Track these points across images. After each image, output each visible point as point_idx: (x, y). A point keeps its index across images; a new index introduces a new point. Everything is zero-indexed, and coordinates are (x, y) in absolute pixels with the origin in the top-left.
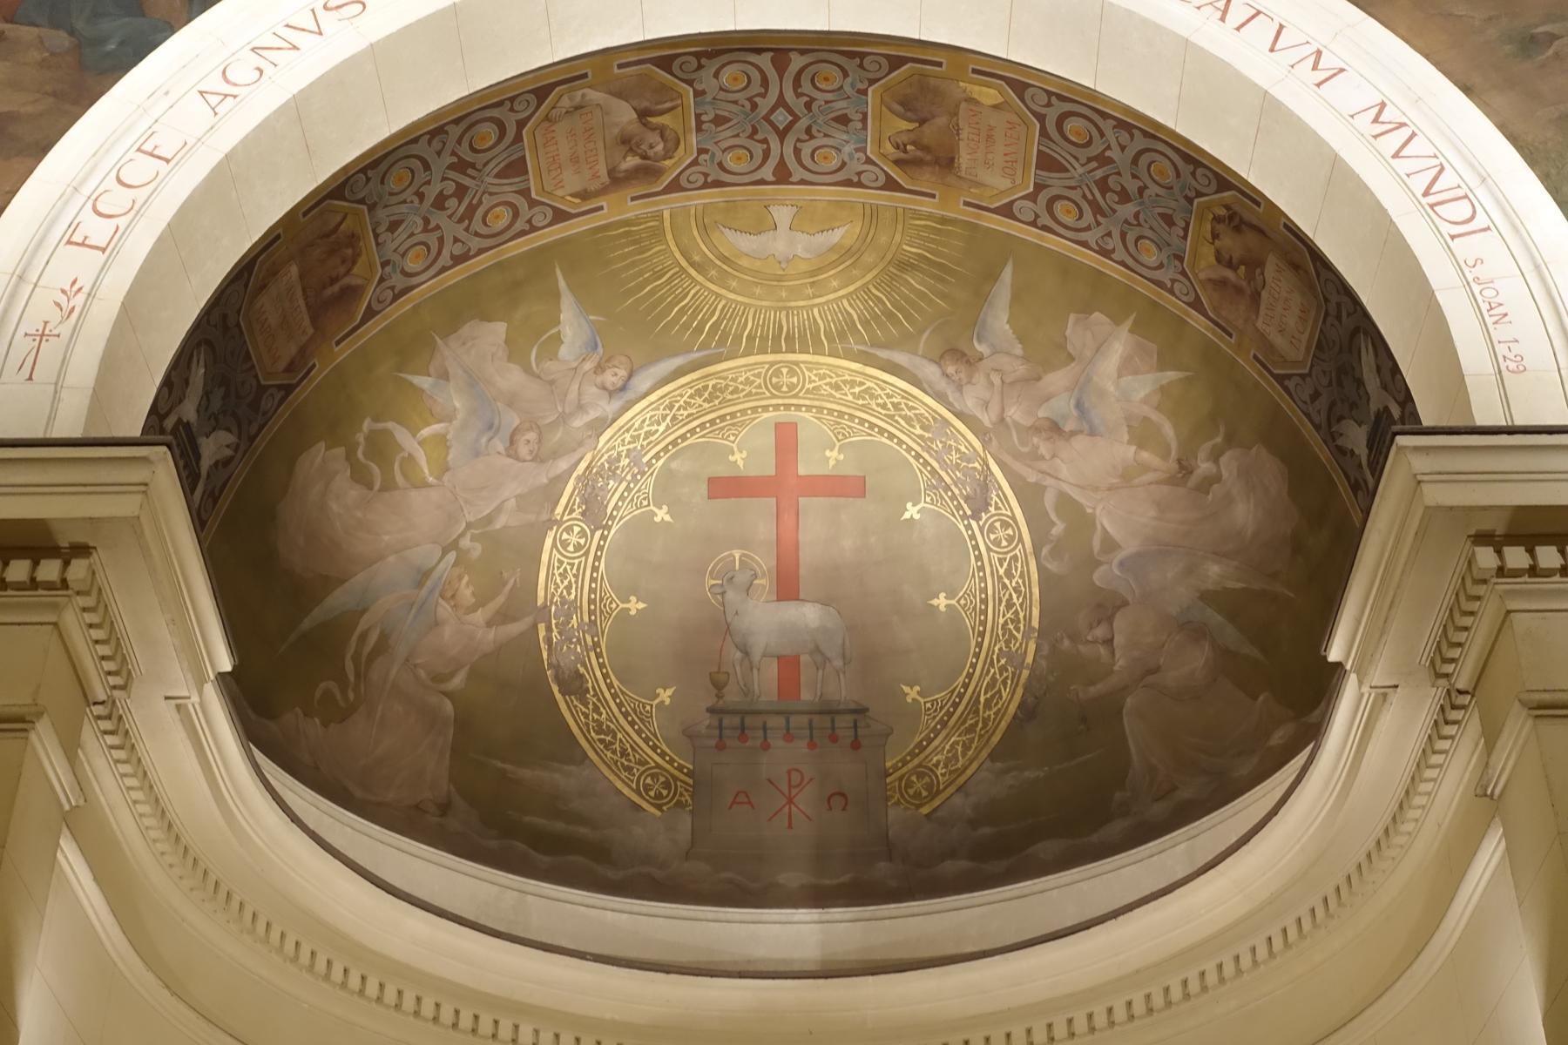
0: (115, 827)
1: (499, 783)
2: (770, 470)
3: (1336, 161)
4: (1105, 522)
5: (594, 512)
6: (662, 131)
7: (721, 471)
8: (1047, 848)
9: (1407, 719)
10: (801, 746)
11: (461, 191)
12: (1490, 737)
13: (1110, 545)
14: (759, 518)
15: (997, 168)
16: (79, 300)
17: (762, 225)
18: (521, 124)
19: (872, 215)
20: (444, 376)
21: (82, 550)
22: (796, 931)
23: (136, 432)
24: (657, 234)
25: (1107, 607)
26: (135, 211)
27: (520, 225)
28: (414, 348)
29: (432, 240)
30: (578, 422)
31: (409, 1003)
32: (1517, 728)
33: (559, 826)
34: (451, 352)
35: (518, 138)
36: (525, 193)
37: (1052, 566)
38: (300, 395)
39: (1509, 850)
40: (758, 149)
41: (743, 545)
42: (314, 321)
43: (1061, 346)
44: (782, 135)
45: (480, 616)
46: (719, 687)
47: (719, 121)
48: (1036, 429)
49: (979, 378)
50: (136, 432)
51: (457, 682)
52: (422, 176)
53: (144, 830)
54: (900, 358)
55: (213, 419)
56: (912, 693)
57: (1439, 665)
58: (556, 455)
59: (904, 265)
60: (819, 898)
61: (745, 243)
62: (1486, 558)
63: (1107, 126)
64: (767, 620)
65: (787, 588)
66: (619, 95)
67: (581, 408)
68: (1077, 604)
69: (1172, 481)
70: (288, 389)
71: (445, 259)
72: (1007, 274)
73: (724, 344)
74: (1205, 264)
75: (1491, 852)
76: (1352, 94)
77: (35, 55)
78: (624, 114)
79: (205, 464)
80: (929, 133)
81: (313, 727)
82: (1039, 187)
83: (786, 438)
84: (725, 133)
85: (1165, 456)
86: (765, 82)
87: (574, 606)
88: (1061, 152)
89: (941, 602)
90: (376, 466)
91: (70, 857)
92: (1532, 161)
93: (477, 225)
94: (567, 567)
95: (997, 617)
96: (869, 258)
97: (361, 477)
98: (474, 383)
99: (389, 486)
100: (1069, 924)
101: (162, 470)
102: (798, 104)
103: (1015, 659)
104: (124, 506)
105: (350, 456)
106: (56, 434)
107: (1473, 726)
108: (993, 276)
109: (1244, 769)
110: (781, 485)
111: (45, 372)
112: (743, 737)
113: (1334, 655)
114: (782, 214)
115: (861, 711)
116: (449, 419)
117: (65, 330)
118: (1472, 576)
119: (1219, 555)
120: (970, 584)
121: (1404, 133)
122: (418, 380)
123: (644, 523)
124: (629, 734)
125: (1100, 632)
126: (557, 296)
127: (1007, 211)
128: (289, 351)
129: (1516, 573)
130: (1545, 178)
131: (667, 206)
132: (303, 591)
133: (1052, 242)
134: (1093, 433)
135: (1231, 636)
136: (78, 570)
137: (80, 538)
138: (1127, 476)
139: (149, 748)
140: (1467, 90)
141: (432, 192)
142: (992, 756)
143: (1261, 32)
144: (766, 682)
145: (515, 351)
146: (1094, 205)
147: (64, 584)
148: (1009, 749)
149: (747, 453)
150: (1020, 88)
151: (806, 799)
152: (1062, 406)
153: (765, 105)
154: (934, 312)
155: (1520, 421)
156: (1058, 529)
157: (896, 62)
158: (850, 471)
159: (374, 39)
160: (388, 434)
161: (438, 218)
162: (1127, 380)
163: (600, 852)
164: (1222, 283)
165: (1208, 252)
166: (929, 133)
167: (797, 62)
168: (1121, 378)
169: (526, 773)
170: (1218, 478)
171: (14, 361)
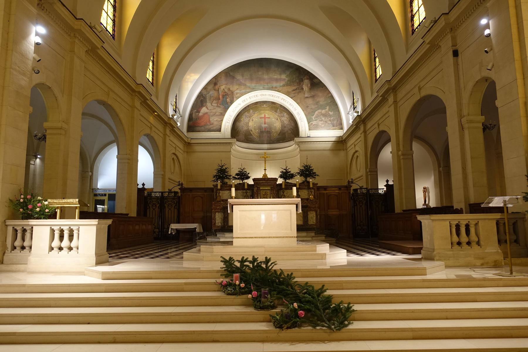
0: (260, 242)
1: (248, 138)
5: (253, 120)
14: (263, 120)
22: (265, 146)
25: (285, 127)
60: (267, 144)
64: (264, 126)
65: (265, 124)
68: (283, 126)
73: (261, 110)
83: (265, 115)
124: (255, 134)
144: (264, 130)
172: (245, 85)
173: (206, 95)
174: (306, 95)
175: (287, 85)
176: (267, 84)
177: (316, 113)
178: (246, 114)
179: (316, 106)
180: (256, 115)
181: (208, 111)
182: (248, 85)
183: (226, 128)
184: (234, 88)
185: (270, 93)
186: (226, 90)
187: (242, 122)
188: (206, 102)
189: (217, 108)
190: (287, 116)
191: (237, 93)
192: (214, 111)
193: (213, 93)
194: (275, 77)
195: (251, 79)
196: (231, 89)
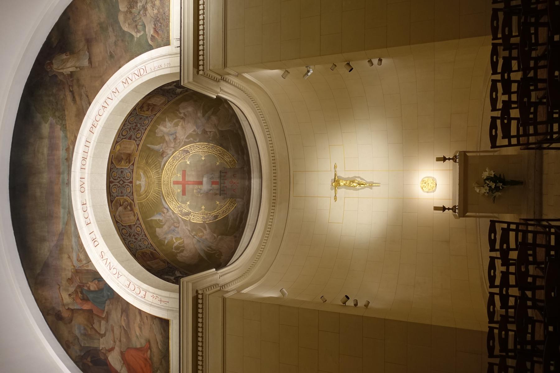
1: (230, 230)
3: (132, 91)
4: (191, 131)
5: (188, 214)
6: (123, 202)
7: (181, 193)
8: (243, 143)
9: (225, 86)
10: (226, 181)
11: (134, 235)
12: (229, 74)
13: (194, 131)
14: (189, 187)
15: (130, 147)
16: (155, 295)
17: (140, 186)
18: (122, 226)
19: (138, 167)
20: (165, 238)
21: (197, 291)
22: (255, 182)
23: (178, 286)
24: (141, 203)
25: (205, 132)
26: (139, 287)
27: (140, 226)
28: (160, 243)
29: (142, 240)
30: (173, 216)
31: (265, 241)
32: (228, 70)
33: (238, 219)
34: (161, 237)
35: (125, 226)
36: (134, 225)
37: (198, 140)
38: (169, 261)
39: (246, 73)
40: (127, 186)
41: (193, 190)
42: (157, 259)
43: (161, 137)
44: (124, 182)
45: (205, 232)
46: (216, 194)
47: (122, 193)
48: (175, 142)
49: (166, 151)
50: (178, 286)
51: (215, 235)
52: (131, 242)
53: (240, 282)
54: (163, 164)
55: (173, 274)
56: (218, 163)
57: (217, 81)
58: (178, 220)
59: (147, 163)
60: (250, 179)
61: (143, 189)
62: (201, 72)
63: (124, 128)
64: (206, 186)
65: (201, 183)
66: (117, 209)
67: (170, 216)
68: (204, 137)
69: (184, 121)
70: (168, 263)
71: (146, 238)
72: (149, 146)
73: (160, 193)
74: (149, 113)
75: (246, 75)
76: (121, 87)
77: (111, 306)
78: (120, 209)
79: (181, 275)
80: (124, 157)
81: (223, 257)
82: (134, 140)
83: (176, 183)
84: (124, 192)
86: (115, 185)
87: (203, 217)
88: (128, 136)
89: (203, 158)
90: (180, 248)
91: (245, 291)
92: (133, 58)
93: (140, 233)
94: (197, 218)
95: (206, 150)
96: (146, 168)
97: (182, 251)
98: (166, 233)
99: (183, 247)
101: (184, 280)
102: (119, 180)
103: (213, 147)
104: (190, 285)
105: (179, 253)
106: (178, 297)
107: (227, 76)
108: (149, 148)
109: (231, 111)
110: (184, 184)
111: (167, 300)
112: (224, 190)
113: (215, 97)
114: (138, 183)
115: (221, 172)
116: (172, 238)
117: (160, 297)
118: (205, 75)
120: (200, 153)
121: (128, 79)
122: (166, 242)
123: (190, 206)
124: (224, 208)
125: (209, 133)
126: (151, 220)
127: (138, 145)
128: (162, 263)
129: (203, 68)
130: (136, 56)
131: (136, 202)
132: (201, 259)
133: (144, 138)
134: (176, 133)
135: (210, 112)
136: (200, 292)
137: (195, 292)
138: (183, 128)
139: (227, 281)
140: (120, 68)
141: (135, 240)
142: (228, 151)
143: (109, 101)
145: (161, 227)
146: (137, 131)
147: (202, 294)
148: (227, 149)
149: (178, 189)
150: (117, 142)
151: (235, 181)
152: (171, 138)
153: (119, 185)
154: (155, 158)
155: (179, 65)
156: (192, 139)
157: (112, 163)
158: (181, 173)
160: (175, 247)
161: (139, 239)
162: (167, 127)
163: (242, 213)
164: (152, 110)
165: (147, 112)
166: (124, 157)
167: (112, 179)
168: (167, 128)
169: (230, 224)
170: (184, 113)
171: (165, 305)
172: (61, 234)
173: (82, 348)
174: (86, 63)
175: (62, 118)
176: (59, 173)
177: (126, 28)
179: (110, 29)
181: (117, 349)
183: (157, 301)
184: (67, 266)
186: (72, 289)
187: (187, 241)
188: (97, 350)
189: (111, 322)
190: (168, 124)
191: (79, 260)
192: (117, 331)
193: (78, 325)
194: (46, 151)
195: (49, 217)
196: (69, 275)
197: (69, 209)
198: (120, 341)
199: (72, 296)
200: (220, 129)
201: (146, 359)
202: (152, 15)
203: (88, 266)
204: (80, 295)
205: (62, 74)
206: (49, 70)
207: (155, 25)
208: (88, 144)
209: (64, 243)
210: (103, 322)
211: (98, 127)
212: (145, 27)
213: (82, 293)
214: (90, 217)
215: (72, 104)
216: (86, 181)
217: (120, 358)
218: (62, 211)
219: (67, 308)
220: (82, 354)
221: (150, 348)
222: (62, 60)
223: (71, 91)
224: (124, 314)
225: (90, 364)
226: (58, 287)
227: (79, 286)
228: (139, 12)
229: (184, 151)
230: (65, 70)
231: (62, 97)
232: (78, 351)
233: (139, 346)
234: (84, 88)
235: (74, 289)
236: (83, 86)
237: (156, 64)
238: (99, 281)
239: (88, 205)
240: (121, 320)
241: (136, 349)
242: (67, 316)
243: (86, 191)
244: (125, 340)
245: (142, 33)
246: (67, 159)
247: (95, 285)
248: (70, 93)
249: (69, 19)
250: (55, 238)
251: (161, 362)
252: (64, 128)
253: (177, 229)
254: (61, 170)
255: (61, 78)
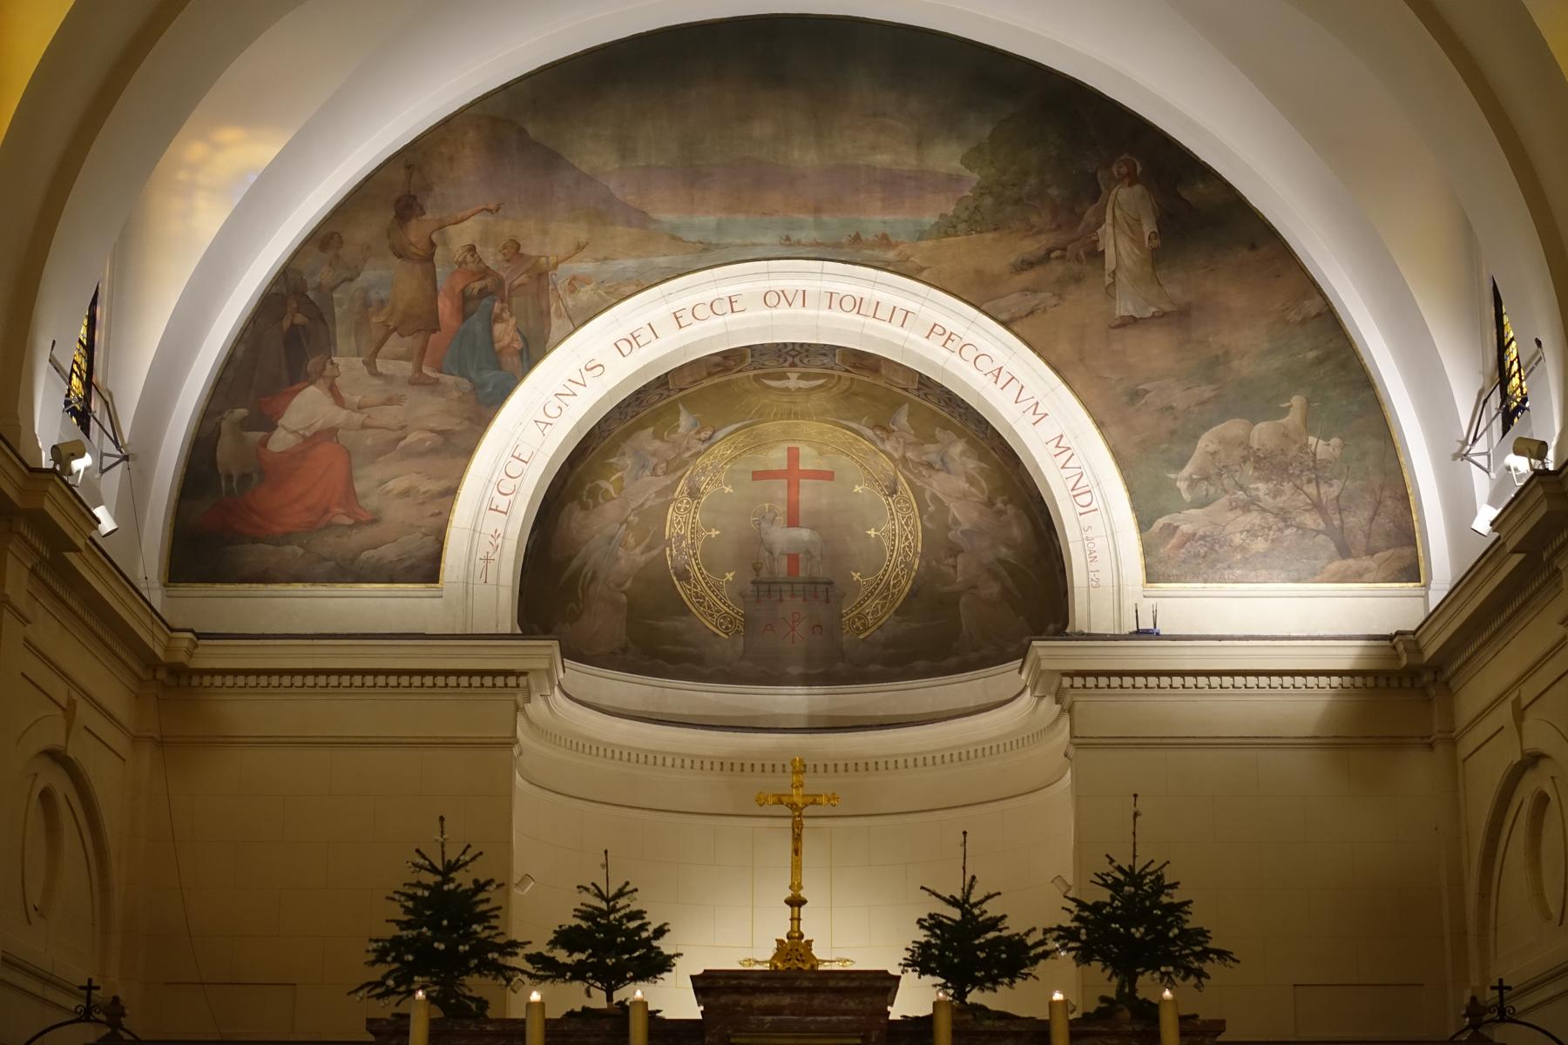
2: (784, 466)
5: (694, 493)
8: (921, 664)
10: (799, 601)
13: (956, 522)
14: (779, 489)
22: (795, 700)
25: (954, 551)
33: (678, 649)
37: (928, 525)
45: (638, 550)
46: (757, 570)
51: (628, 585)
56: (856, 576)
60: (807, 680)
64: (781, 536)
65: (793, 521)
68: (941, 545)
77: (456, 395)
83: (793, 455)
85: (983, 492)
87: (683, 537)
89: (872, 533)
94: (679, 521)
100: (928, 709)
112: (770, 596)
115: (831, 583)
119: (1008, 546)
124: (712, 600)
134: (949, 472)
136: (523, 680)
138: (965, 496)
140: (1100, 425)
142: (897, 613)
144: (782, 568)
156: (932, 508)
159: (610, 387)
169: (662, 624)
172: (641, 219)
174: (1125, 307)
176: (817, 210)
177: (1206, 442)
178: (646, 440)
179: (1207, 391)
180: (722, 450)
181: (340, 416)
182: (667, 216)
183: (484, 548)
184: (554, 239)
185: (842, 287)
186: (491, 257)
187: (610, 510)
188: (328, 347)
190: (972, 464)
191: (574, 284)
194: (882, 159)
195: (691, 176)
196: (530, 249)
197: (717, 246)
198: (364, 427)
199: (469, 259)
200: (963, 600)
201: (326, 511)
202: (1229, 529)
203: (560, 316)
204: (477, 286)
205: (1099, 224)
206: (1114, 169)
207: (1203, 538)
208: (899, 316)
209: (620, 229)
210: (408, 367)
211: (944, 352)
212: (1202, 506)
213: (483, 293)
214: (697, 326)
215: (1013, 259)
216: (797, 309)
217: (318, 426)
218: (711, 220)
219: (434, 237)
220: (311, 294)
221: (358, 524)
222: (1138, 221)
223: (1050, 251)
224: (439, 439)
225: (286, 324)
226: (492, 206)
227: (500, 283)
228: (1241, 488)
229: (895, 482)
230: (1109, 230)
231: (1034, 219)
232: (317, 279)
233: (359, 487)
234: (1054, 301)
235: (489, 264)
236: (1060, 296)
237: (1101, 544)
238: (520, 352)
239: (730, 317)
240: (423, 429)
241: (349, 480)
242: (413, 240)
243: (767, 312)
244: (369, 442)
245: (1187, 496)
246: (857, 238)
247: (507, 339)
248: (1042, 252)
249: (1253, 247)
250: (631, 199)
251: (326, 560)
252: (947, 228)
253: (648, 472)
254: (825, 218)
255: (1090, 215)
